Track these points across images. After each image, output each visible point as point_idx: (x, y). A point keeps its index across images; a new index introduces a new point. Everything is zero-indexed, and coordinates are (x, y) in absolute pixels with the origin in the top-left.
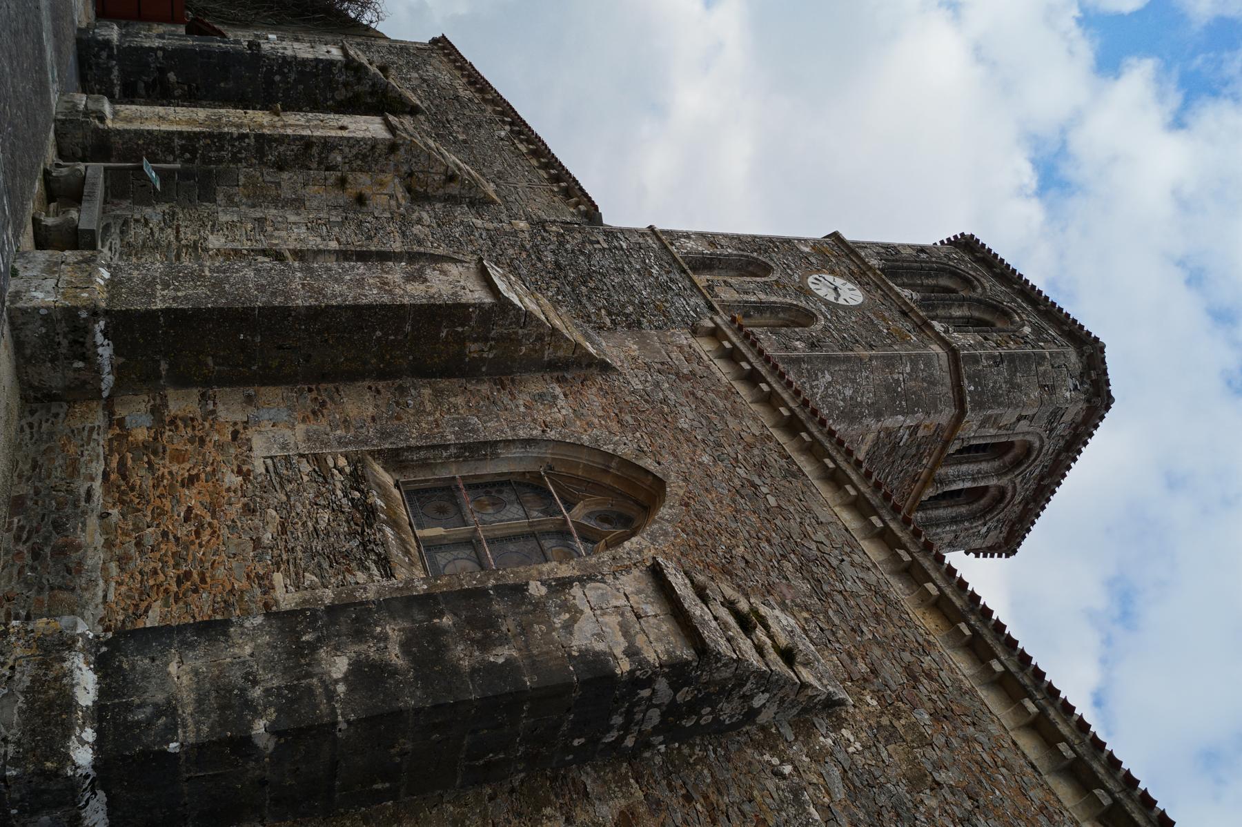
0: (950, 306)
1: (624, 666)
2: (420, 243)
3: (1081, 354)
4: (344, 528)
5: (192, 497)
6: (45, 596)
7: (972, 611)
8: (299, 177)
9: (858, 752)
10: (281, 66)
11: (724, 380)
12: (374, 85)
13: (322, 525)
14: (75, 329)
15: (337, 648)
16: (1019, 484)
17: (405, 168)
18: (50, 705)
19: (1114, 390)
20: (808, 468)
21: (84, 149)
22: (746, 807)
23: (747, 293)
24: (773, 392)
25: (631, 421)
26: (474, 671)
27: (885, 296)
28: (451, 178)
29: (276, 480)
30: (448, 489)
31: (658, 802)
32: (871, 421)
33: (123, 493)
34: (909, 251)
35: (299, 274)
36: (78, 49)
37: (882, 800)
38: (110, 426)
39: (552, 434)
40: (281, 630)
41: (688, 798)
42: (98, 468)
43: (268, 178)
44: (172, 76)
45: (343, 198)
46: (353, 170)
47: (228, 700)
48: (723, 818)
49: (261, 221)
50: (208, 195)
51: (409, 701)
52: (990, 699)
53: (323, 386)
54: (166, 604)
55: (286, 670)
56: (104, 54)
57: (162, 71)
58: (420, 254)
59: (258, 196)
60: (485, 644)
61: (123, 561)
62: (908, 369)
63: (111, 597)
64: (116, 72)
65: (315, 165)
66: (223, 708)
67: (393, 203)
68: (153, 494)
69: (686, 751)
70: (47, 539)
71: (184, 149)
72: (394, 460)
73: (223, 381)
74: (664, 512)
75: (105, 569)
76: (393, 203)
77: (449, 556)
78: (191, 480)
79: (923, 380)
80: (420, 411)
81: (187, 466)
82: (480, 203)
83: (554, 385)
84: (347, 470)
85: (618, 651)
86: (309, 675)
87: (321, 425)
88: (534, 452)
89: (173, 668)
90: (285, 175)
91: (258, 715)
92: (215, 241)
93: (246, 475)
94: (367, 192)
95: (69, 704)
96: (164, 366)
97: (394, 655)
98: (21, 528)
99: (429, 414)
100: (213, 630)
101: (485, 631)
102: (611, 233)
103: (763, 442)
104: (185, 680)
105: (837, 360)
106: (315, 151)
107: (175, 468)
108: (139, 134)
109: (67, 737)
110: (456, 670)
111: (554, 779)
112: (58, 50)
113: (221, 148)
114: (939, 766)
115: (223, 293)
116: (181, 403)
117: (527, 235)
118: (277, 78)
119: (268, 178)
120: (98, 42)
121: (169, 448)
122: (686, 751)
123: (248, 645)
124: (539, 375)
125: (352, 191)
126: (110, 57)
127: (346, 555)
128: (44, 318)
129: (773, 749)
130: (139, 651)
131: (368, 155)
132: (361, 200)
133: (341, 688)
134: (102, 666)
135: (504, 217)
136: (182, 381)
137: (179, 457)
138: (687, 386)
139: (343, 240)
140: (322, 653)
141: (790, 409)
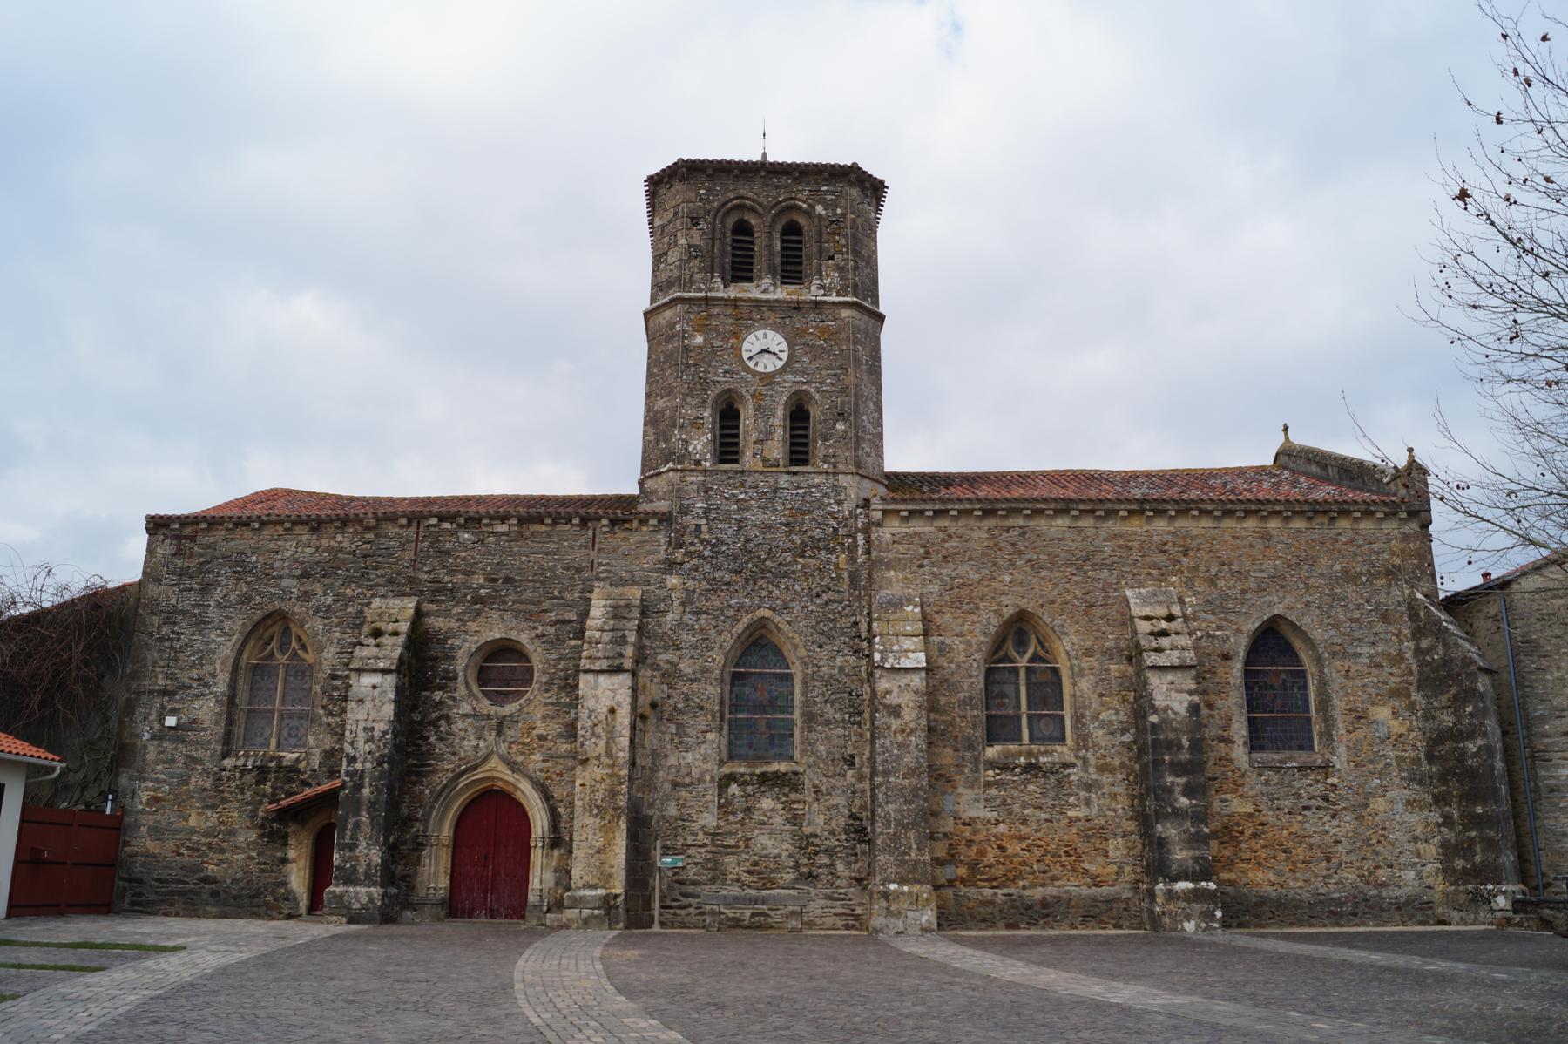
2: (704, 670)
5: (1014, 848)
19: (846, 161)
20: (1020, 522)
24: (959, 511)
27: (771, 309)
42: (988, 892)
49: (675, 785)
60: (1180, 747)
61: (1054, 878)
68: (1009, 866)
80: (952, 723)
87: (960, 779)
92: (709, 819)
93: (997, 823)
94: (649, 701)
95: (1195, 890)
114: (1208, 571)
125: (648, 711)
132: (654, 705)
134: (1175, 880)
137: (982, 853)
138: (937, 558)
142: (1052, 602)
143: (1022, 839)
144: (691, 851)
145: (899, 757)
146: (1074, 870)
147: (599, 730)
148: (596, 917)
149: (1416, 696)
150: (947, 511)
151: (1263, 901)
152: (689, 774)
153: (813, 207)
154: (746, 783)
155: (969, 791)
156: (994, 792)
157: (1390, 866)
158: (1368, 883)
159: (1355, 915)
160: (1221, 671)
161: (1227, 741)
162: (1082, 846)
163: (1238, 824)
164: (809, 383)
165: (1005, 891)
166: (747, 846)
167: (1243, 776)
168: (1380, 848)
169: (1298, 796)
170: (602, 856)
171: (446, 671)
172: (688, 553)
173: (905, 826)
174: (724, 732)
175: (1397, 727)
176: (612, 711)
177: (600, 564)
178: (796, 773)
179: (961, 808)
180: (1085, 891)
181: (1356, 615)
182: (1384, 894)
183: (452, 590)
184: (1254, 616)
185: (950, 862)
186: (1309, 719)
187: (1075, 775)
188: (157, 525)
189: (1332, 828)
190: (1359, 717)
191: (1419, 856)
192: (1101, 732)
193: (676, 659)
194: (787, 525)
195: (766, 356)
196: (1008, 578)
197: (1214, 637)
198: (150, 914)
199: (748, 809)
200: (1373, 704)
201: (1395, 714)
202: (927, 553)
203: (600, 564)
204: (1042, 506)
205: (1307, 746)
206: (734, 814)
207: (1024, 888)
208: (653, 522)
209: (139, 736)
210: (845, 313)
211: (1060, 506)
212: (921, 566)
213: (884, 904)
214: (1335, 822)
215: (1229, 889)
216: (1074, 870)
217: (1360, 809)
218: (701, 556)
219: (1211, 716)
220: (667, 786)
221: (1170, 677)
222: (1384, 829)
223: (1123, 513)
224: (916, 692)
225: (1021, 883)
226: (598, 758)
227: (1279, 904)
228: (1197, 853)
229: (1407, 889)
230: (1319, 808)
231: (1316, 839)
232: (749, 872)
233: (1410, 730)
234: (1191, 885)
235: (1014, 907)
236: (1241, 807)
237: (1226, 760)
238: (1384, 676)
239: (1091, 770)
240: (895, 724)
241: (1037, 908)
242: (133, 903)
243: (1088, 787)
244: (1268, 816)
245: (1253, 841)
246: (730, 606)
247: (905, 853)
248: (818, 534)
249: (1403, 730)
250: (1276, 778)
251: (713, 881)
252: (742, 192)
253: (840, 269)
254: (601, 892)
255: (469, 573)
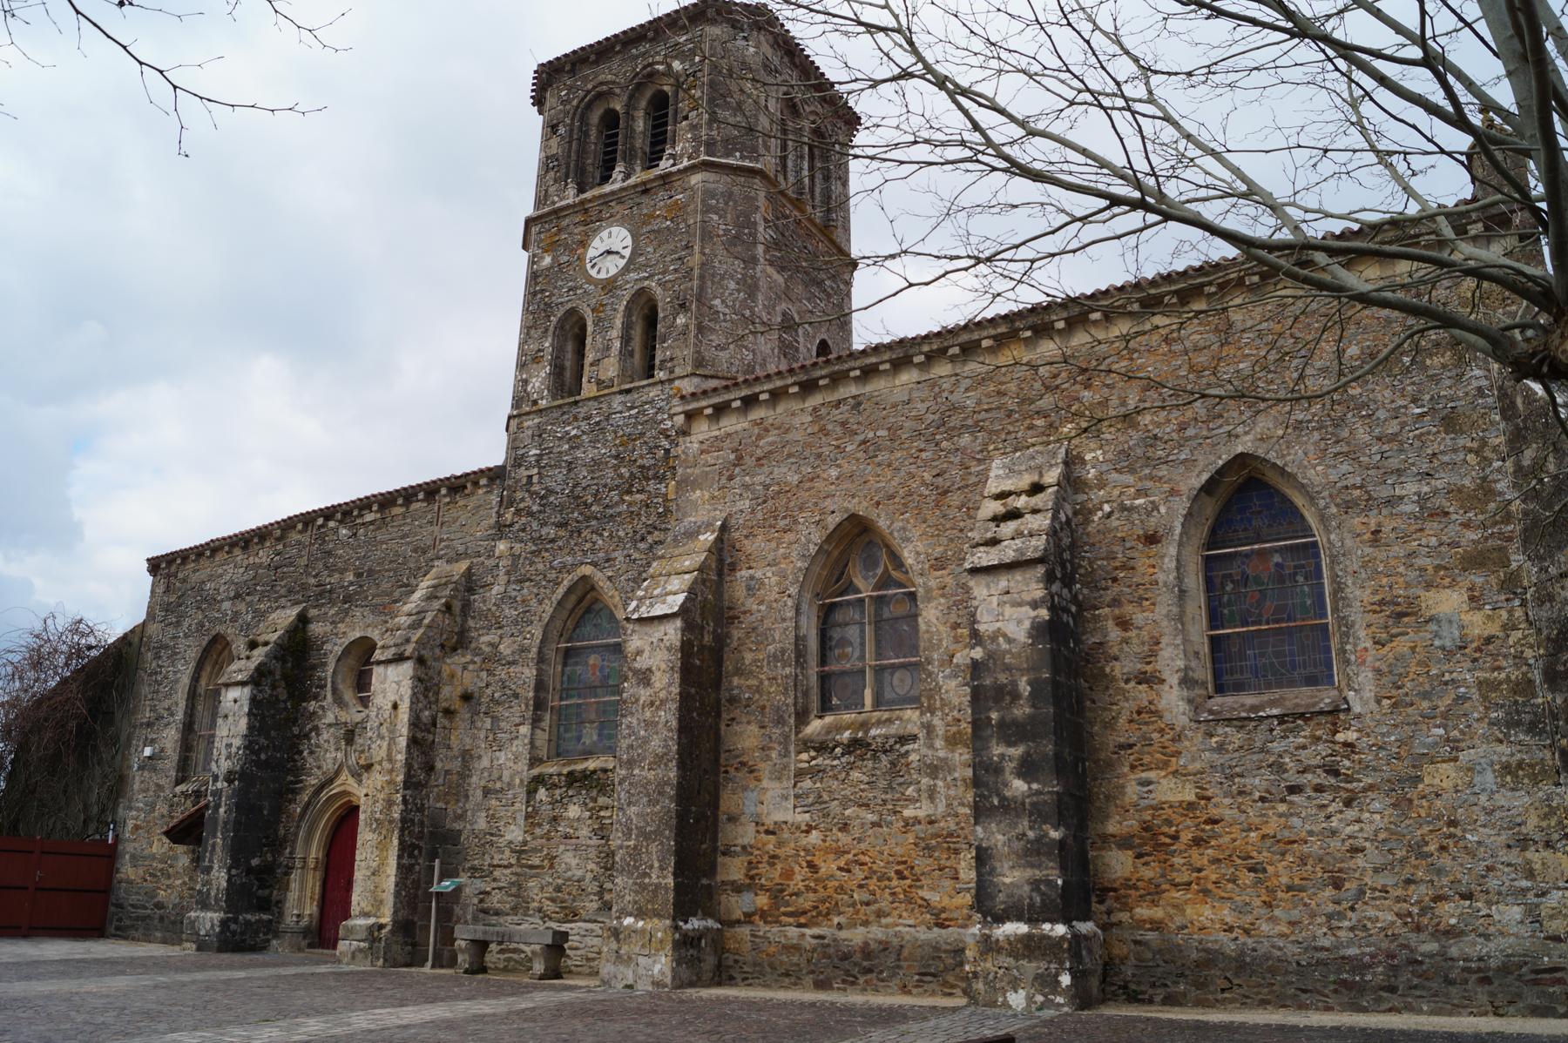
0: (633, 130)
1: (1044, 613)
2: (524, 650)
3: (713, 22)
4: (870, 764)
5: (828, 866)
6: (904, 964)
7: (1012, 321)
8: (442, 752)
9: (1104, 453)
10: (253, 752)
11: (746, 425)
12: (275, 658)
13: (866, 779)
14: (685, 943)
15: (1006, 785)
16: (812, 105)
17: (437, 651)
18: (1027, 947)
21: (406, 944)
22: (1128, 545)
23: (608, 348)
24: (771, 392)
25: (787, 521)
26: (1033, 706)
27: (620, 201)
28: (448, 607)
29: (818, 807)
30: (824, 678)
31: (1114, 600)
32: (759, 268)
33: (819, 914)
34: (554, 142)
35: (636, 771)
36: (226, 951)
37: (1139, 452)
38: (751, 923)
39: (793, 590)
40: (988, 816)
41: (1115, 580)
42: (793, 932)
43: (441, 781)
44: (255, 862)
45: (464, 713)
46: (437, 701)
47: (1033, 851)
48: (1132, 563)
49: (487, 792)
50: (453, 837)
51: (1050, 748)
52: (1080, 339)
53: (722, 761)
54: (921, 887)
55: (1018, 816)
56: (233, 927)
57: (249, 871)
58: (540, 652)
59: (458, 791)
60: (1015, 696)
61: (880, 914)
62: (715, 217)
63: (911, 922)
64: (249, 917)
65: (431, 737)
66: (1039, 854)
67: (471, 667)
68: (822, 893)
69: (1082, 571)
70: (855, 964)
71: (411, 856)
72: (802, 717)
73: (715, 839)
74: (883, 523)
75: (887, 926)
76: (471, 667)
77: (887, 689)
78: (812, 866)
79: (726, 204)
80: (758, 690)
81: (797, 868)
82: (470, 584)
83: (738, 574)
84: (813, 753)
85: (1033, 614)
86: (1023, 804)
87: (765, 768)
88: (805, 607)
89: (1007, 880)
90: (439, 765)
91: (1046, 835)
93: (809, 829)
94: (459, 691)
95: (1028, 937)
96: (705, 881)
97: (1017, 751)
98: (844, 981)
99: (761, 682)
100: (983, 857)
101: (1004, 694)
102: (516, 457)
103: (820, 418)
104: (1017, 873)
105: (702, 288)
106: (419, 735)
107: (799, 877)
108: (397, 894)
109: (1049, 937)
110: (1031, 717)
111: (1088, 662)
112: (219, 967)
113: (412, 821)
114: (1123, 403)
115: (657, 832)
116: (734, 869)
117: (518, 546)
118: (263, 757)
119: (441, 781)
120: (222, 932)
121: (778, 880)
122: (1082, 571)
123: (997, 836)
124: (726, 586)
125: (457, 705)
126: (235, 921)
127: (893, 764)
128: (679, 964)
129: (1092, 512)
130: (993, 898)
131: (425, 686)
132: (467, 697)
133: (1035, 786)
134: (1000, 919)
135: (490, 563)
136: (712, 870)
137: (788, 874)
138: (749, 462)
139: (518, 720)
140: (1008, 794)
141: (793, 384)
142: (892, 497)
143: (840, 852)
144: (497, 873)
145: (646, 741)
146: (910, 901)
147: (384, 730)
148: (361, 950)
149: (1517, 559)
150: (756, 395)
151: (1210, 958)
152: (500, 778)
153: (669, 66)
154: (555, 786)
155: (776, 784)
156: (807, 784)
157: (1468, 896)
158: (1418, 929)
159: (1392, 989)
160: (1142, 564)
161: (1150, 679)
162: (922, 863)
163: (1169, 822)
164: (651, 277)
165: (816, 931)
166: (552, 866)
167: (1178, 738)
168: (1445, 861)
169: (1278, 767)
170: (376, 879)
171: (320, 679)
172: (518, 512)
173: (646, 836)
174: (546, 724)
175: (1478, 624)
176: (395, 706)
177: (442, 540)
178: (605, 771)
179: (763, 809)
180: (923, 934)
181: (1393, 427)
182: (1454, 951)
183: (330, 592)
184: (1201, 464)
185: (749, 887)
186: (1325, 627)
187: (915, 753)
188: (155, 565)
189: (1343, 822)
190: (1400, 613)
191: (1530, 874)
192: (953, 683)
193: (497, 639)
194: (617, 457)
195: (610, 257)
196: (834, 473)
197: (1131, 509)
198: (125, 938)
199: (555, 819)
200: (1429, 586)
201: (1475, 601)
202: (739, 458)
203: (442, 540)
204: (873, 360)
205: (1320, 676)
206: (540, 825)
207: (840, 927)
208: (483, 482)
209: (130, 767)
210: (695, 179)
211: (899, 353)
212: (731, 478)
213: (614, 946)
214: (1351, 814)
215: (1150, 936)
216: (910, 901)
217: (1402, 789)
218: (531, 514)
219: (1126, 641)
220: (479, 793)
221: (1003, 582)
222: (1453, 823)
223: (985, 343)
224: (669, 649)
225: (836, 920)
226: (380, 763)
227: (1241, 964)
228: (1038, 873)
229: (1503, 942)
230: (1319, 789)
231: (1314, 847)
232: (553, 900)
233: (1509, 627)
234: (1023, 928)
235: (827, 956)
236: (1171, 791)
237: (1149, 712)
238: (1452, 531)
239: (939, 743)
240: (644, 694)
241: (857, 957)
242: (117, 928)
243: (934, 770)
244: (1223, 807)
245: (1194, 852)
246: (552, 568)
247: (645, 875)
248: (647, 462)
249: (1494, 629)
250: (1236, 738)
251: (515, 910)
252: (602, 78)
253: (693, 127)
254: (372, 921)
255: (342, 571)
